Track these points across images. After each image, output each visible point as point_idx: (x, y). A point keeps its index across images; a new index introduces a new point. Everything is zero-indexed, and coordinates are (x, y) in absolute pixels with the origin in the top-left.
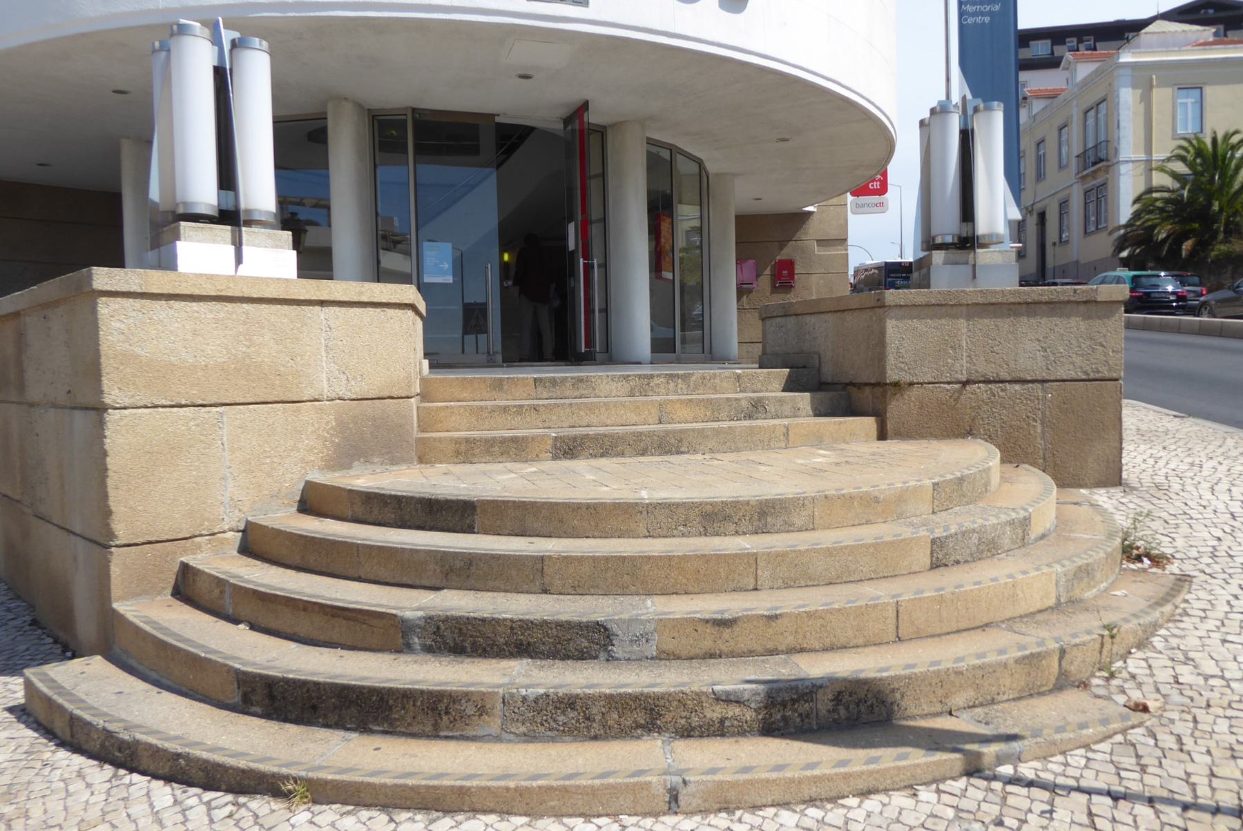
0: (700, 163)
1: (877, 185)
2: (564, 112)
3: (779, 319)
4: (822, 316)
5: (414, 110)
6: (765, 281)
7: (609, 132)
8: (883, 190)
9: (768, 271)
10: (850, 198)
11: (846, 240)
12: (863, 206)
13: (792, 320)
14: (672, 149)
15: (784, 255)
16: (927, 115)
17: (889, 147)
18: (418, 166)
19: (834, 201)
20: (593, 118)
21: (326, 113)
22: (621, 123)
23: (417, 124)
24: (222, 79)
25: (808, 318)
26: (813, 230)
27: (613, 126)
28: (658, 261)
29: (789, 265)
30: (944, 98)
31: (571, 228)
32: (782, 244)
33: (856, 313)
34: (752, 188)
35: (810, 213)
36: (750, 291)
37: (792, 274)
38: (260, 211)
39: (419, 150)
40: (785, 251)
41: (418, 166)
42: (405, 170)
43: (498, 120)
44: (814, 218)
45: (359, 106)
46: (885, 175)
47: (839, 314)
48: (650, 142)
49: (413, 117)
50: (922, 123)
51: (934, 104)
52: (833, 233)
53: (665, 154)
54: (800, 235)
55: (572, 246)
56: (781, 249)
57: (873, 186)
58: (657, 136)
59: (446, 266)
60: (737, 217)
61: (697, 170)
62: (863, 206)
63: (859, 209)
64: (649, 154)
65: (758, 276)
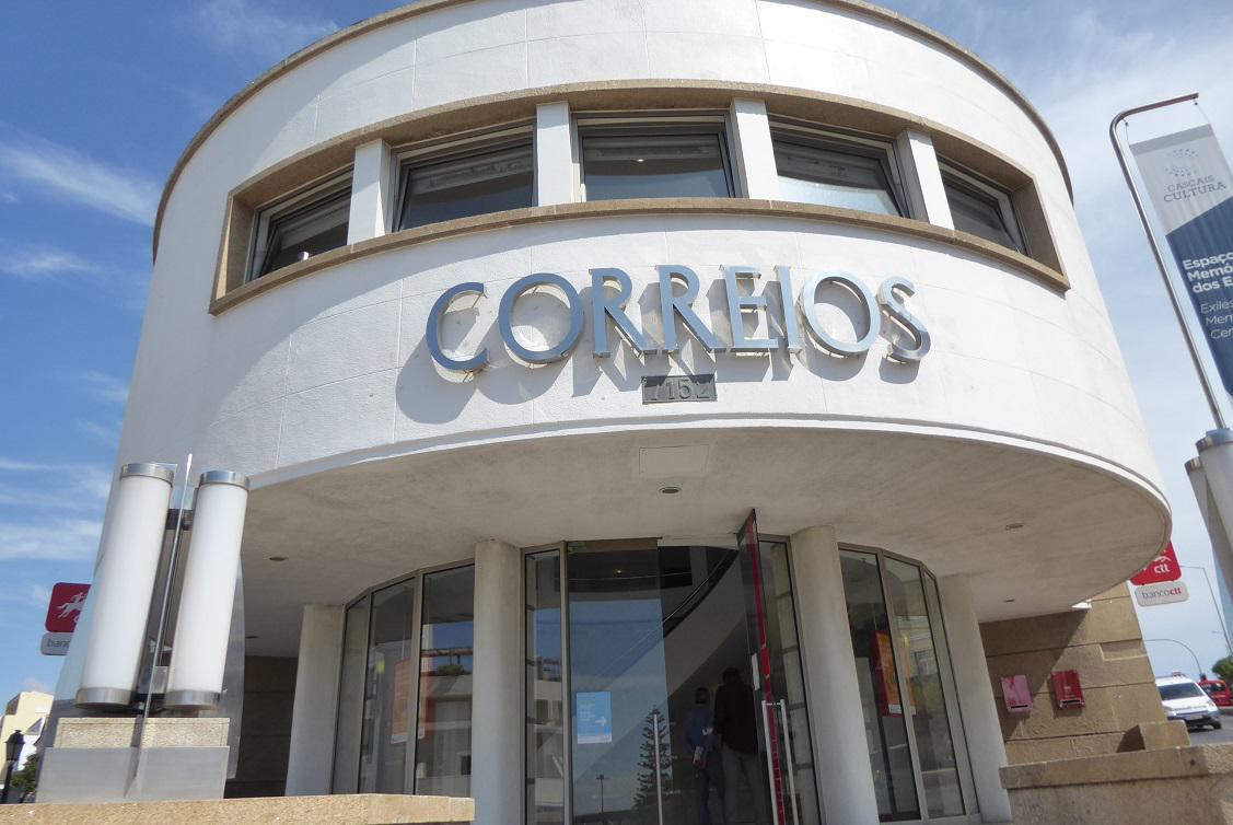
0: (919, 566)
1: (1165, 569)
2: (734, 526)
3: (1027, 794)
4: (1097, 789)
5: (567, 544)
6: (1043, 702)
7: (794, 543)
8: (1174, 572)
9: (1044, 688)
10: (1132, 588)
11: (1140, 640)
12: (1153, 595)
13: (1048, 793)
14: (878, 554)
15: (1062, 664)
16: (1194, 454)
17: (1163, 519)
18: (573, 604)
19: (1112, 592)
20: (763, 527)
21: (473, 559)
22: (806, 530)
23: (571, 559)
24: (179, 524)
25: (1072, 793)
26: (1090, 632)
27: (796, 534)
28: (879, 696)
29: (1072, 677)
30: (1214, 427)
31: (754, 659)
32: (1056, 653)
33: (1157, 787)
34: (1002, 584)
35: (1083, 612)
36: (1026, 716)
37: (1077, 690)
38: (194, 693)
39: (571, 587)
40: (1061, 660)
41: (571, 604)
42: (555, 615)
43: (660, 543)
44: (1090, 613)
45: (508, 546)
46: (1170, 552)
47: (1126, 787)
48: (843, 547)
49: (567, 551)
50: (1189, 467)
51: (1203, 435)
52: (1121, 633)
53: (871, 560)
54: (1075, 639)
55: (757, 685)
56: (1056, 658)
57: (1161, 569)
58: (854, 541)
59: (604, 721)
60: (980, 624)
61: (917, 573)
62: (1153, 595)
63: (1147, 600)
64: (845, 563)
65: (1033, 695)
